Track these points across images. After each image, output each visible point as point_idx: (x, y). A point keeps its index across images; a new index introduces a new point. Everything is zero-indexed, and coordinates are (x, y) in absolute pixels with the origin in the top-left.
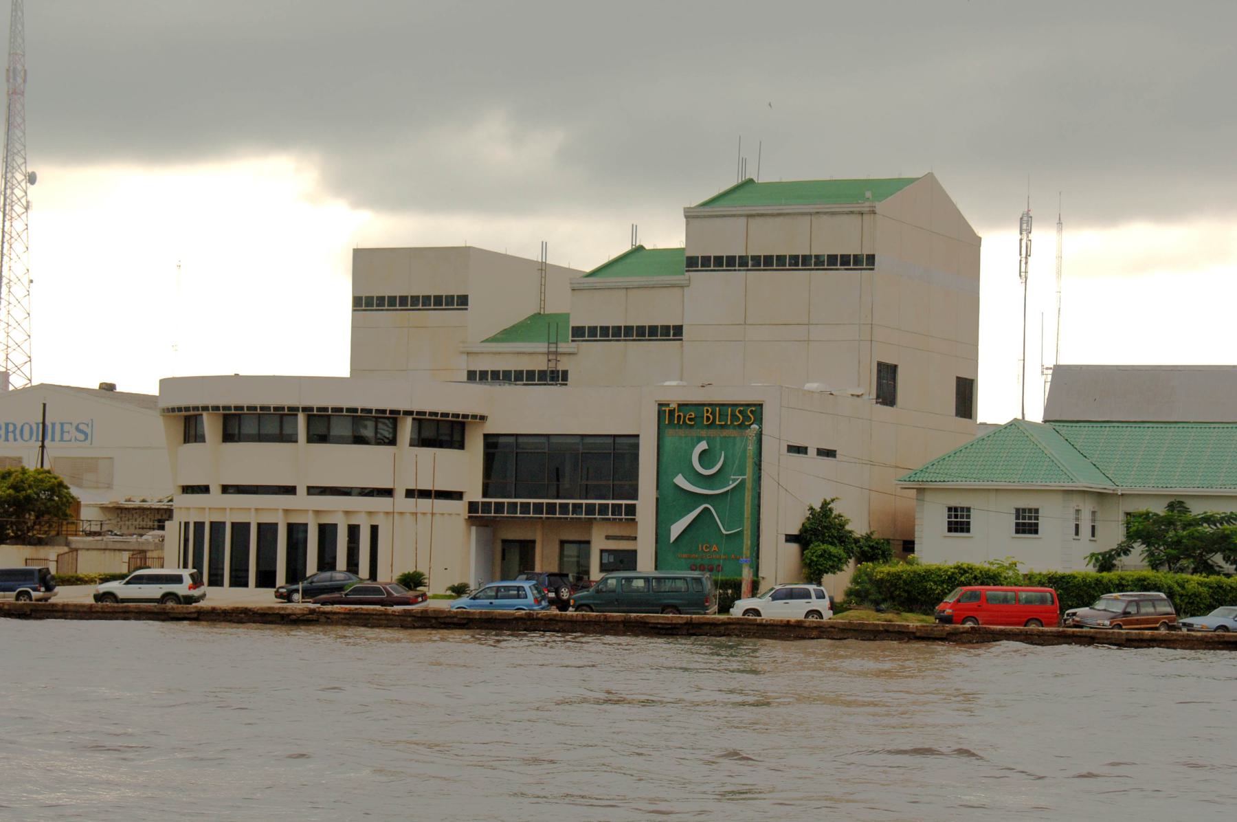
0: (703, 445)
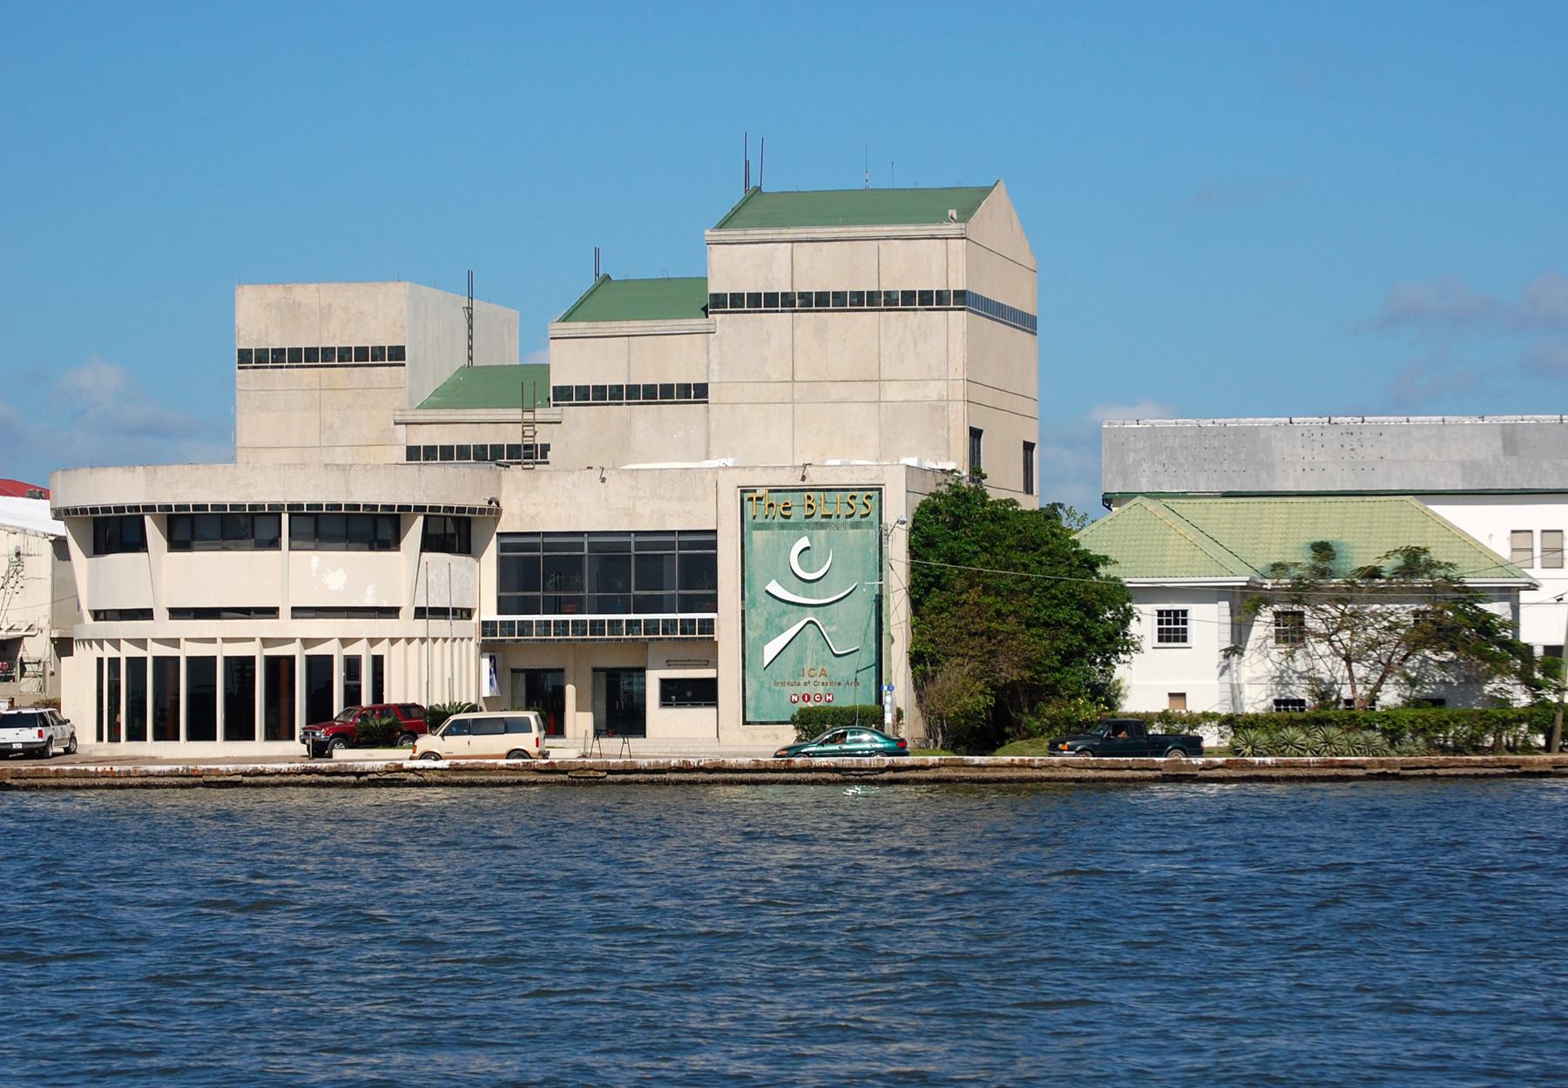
0: (804, 542)
